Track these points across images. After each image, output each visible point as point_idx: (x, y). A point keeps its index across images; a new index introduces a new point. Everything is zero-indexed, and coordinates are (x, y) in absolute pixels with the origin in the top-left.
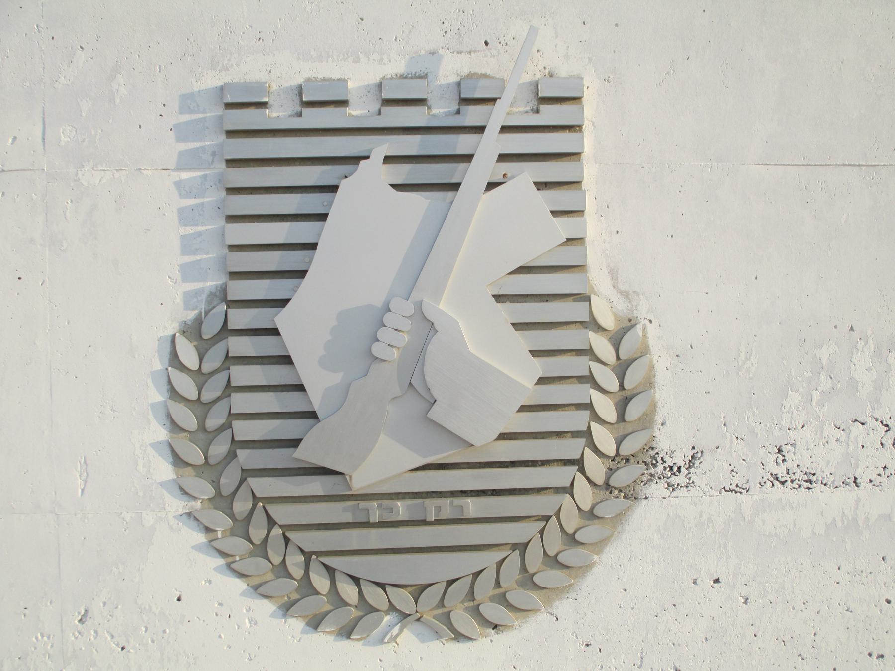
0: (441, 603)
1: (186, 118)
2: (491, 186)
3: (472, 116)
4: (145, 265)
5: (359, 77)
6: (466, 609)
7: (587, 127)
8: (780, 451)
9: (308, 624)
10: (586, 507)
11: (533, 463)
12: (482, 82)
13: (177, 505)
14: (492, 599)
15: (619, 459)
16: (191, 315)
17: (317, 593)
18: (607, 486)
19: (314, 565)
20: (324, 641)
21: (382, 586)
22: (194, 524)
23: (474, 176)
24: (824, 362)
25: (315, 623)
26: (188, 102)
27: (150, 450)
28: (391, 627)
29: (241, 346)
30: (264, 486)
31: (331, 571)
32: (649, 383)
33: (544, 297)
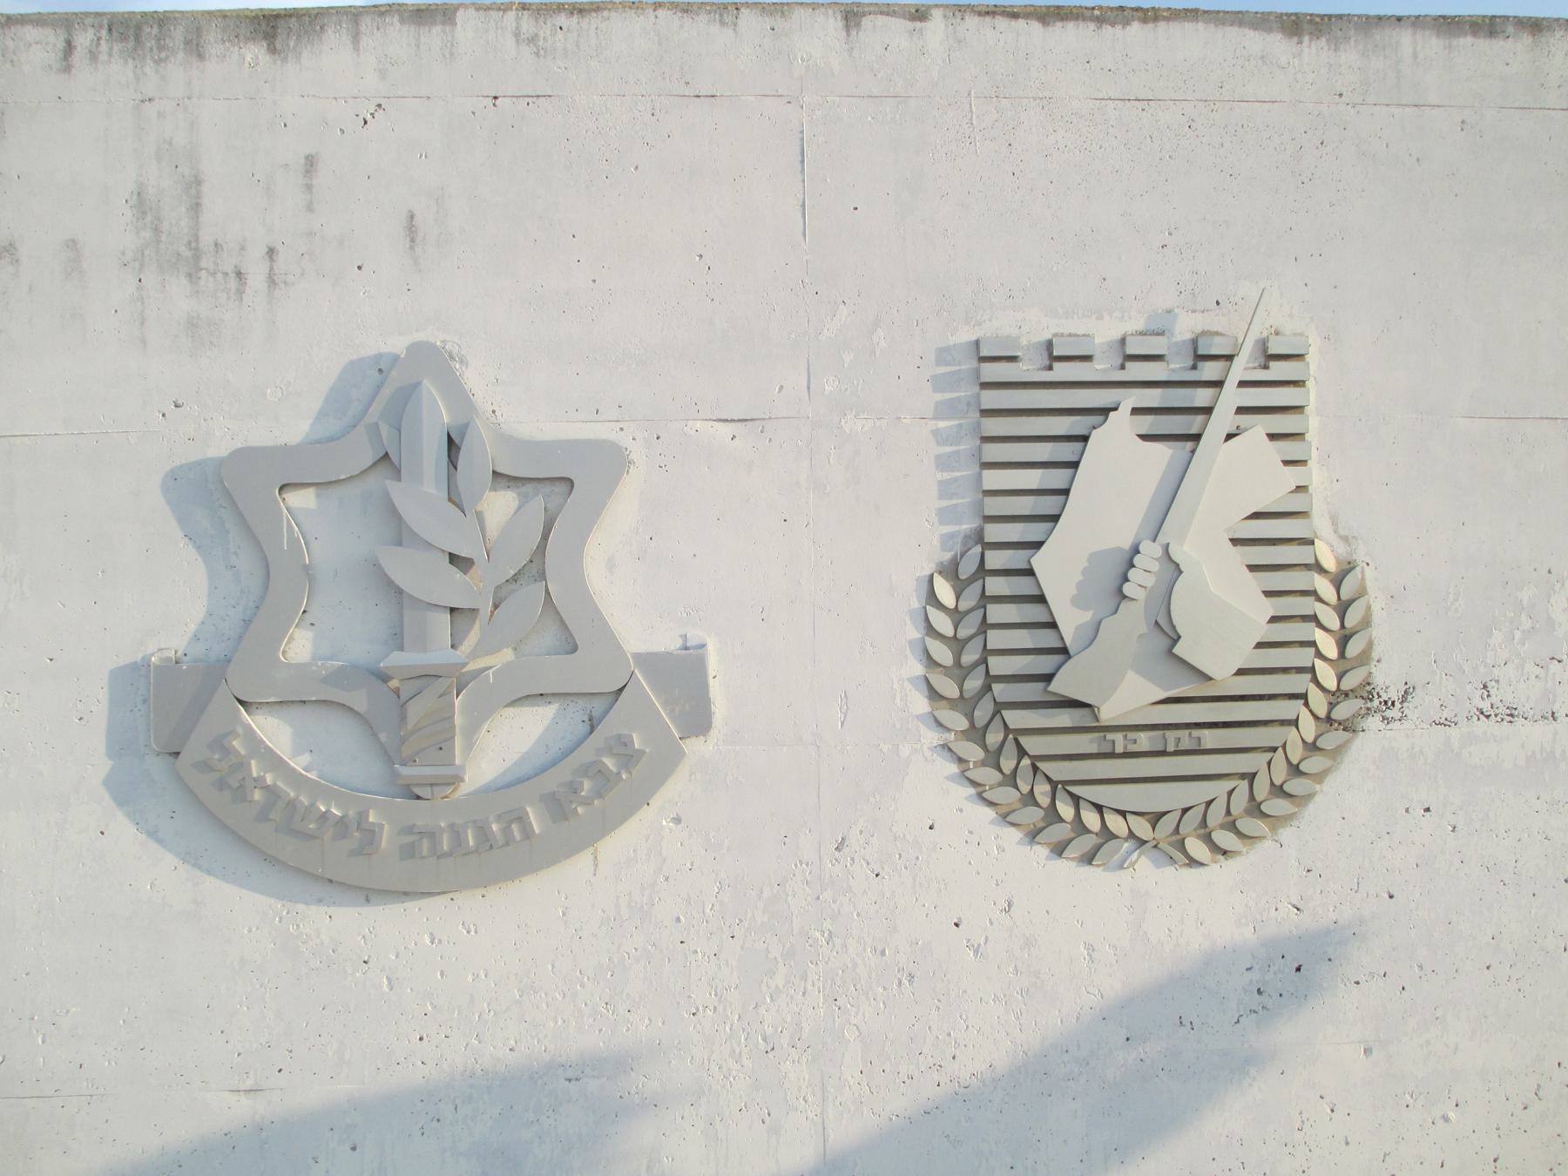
0: (1177, 830)
1: (942, 370)
2: (1230, 437)
3: (1209, 371)
4: (906, 528)
5: (1104, 333)
6: (1199, 837)
7: (1310, 384)
8: (1485, 687)
9: (1052, 851)
10: (1310, 739)
11: (1261, 697)
12: (1217, 339)
13: (932, 737)
14: (1222, 827)
15: (1340, 695)
16: (948, 556)
17: (1062, 820)
18: (1329, 719)
19: (1060, 794)
20: (1066, 868)
21: (1123, 813)
22: (946, 754)
23: (1223, 418)
24: (1525, 602)
25: (1059, 850)
26: (943, 356)
27: (907, 684)
28: (1130, 853)
29: (996, 586)
30: (1015, 719)
31: (1076, 800)
32: (1366, 622)
33: (1270, 541)
